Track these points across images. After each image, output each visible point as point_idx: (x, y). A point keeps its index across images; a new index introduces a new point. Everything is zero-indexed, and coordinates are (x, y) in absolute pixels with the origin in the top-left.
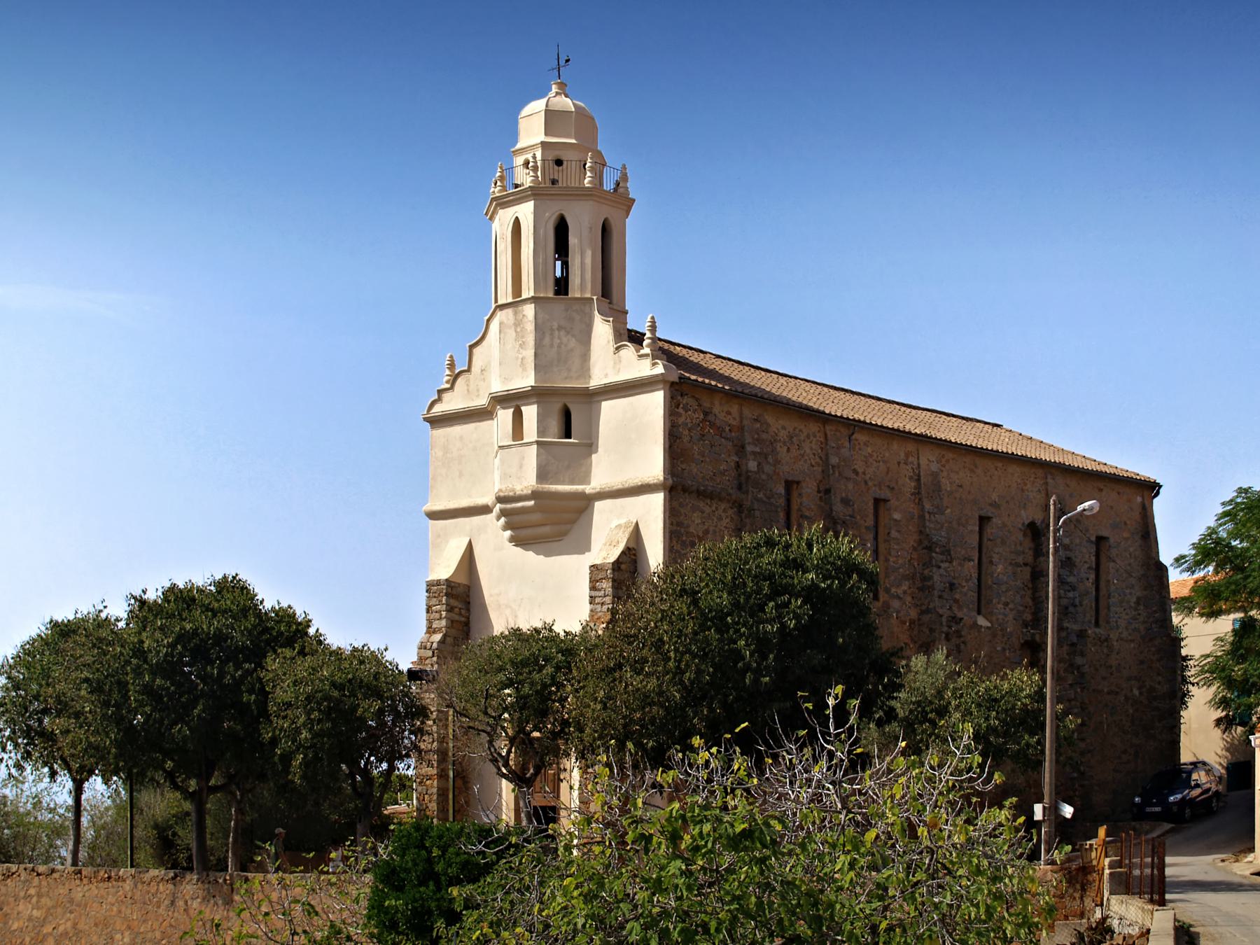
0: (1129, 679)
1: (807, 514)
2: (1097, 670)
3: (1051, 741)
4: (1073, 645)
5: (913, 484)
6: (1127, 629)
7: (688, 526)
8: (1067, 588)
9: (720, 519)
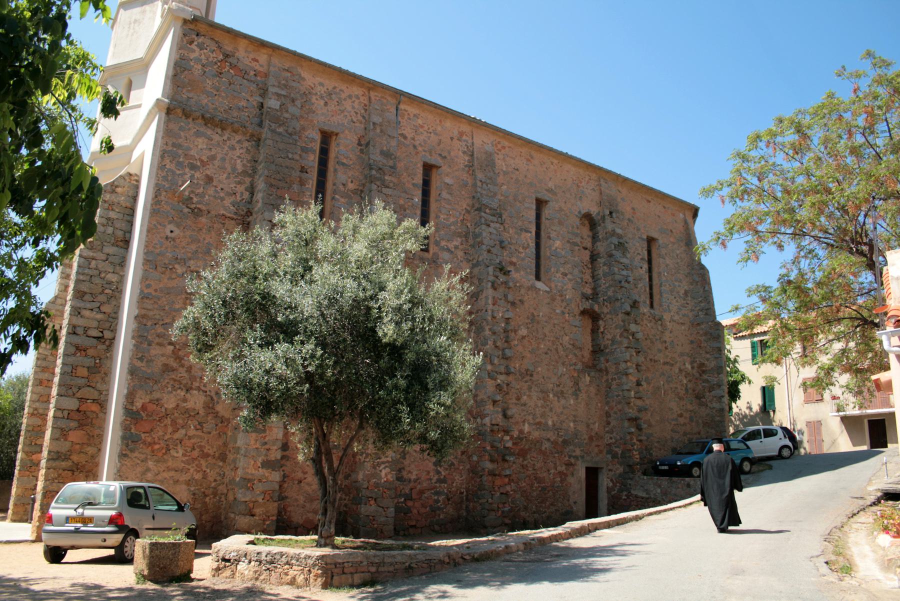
0: (682, 355)
1: (345, 161)
2: (652, 342)
3: (142, 226)
4: (628, 314)
5: (467, 158)
6: (677, 313)
7: (189, 149)
8: (621, 266)
9: (233, 148)
